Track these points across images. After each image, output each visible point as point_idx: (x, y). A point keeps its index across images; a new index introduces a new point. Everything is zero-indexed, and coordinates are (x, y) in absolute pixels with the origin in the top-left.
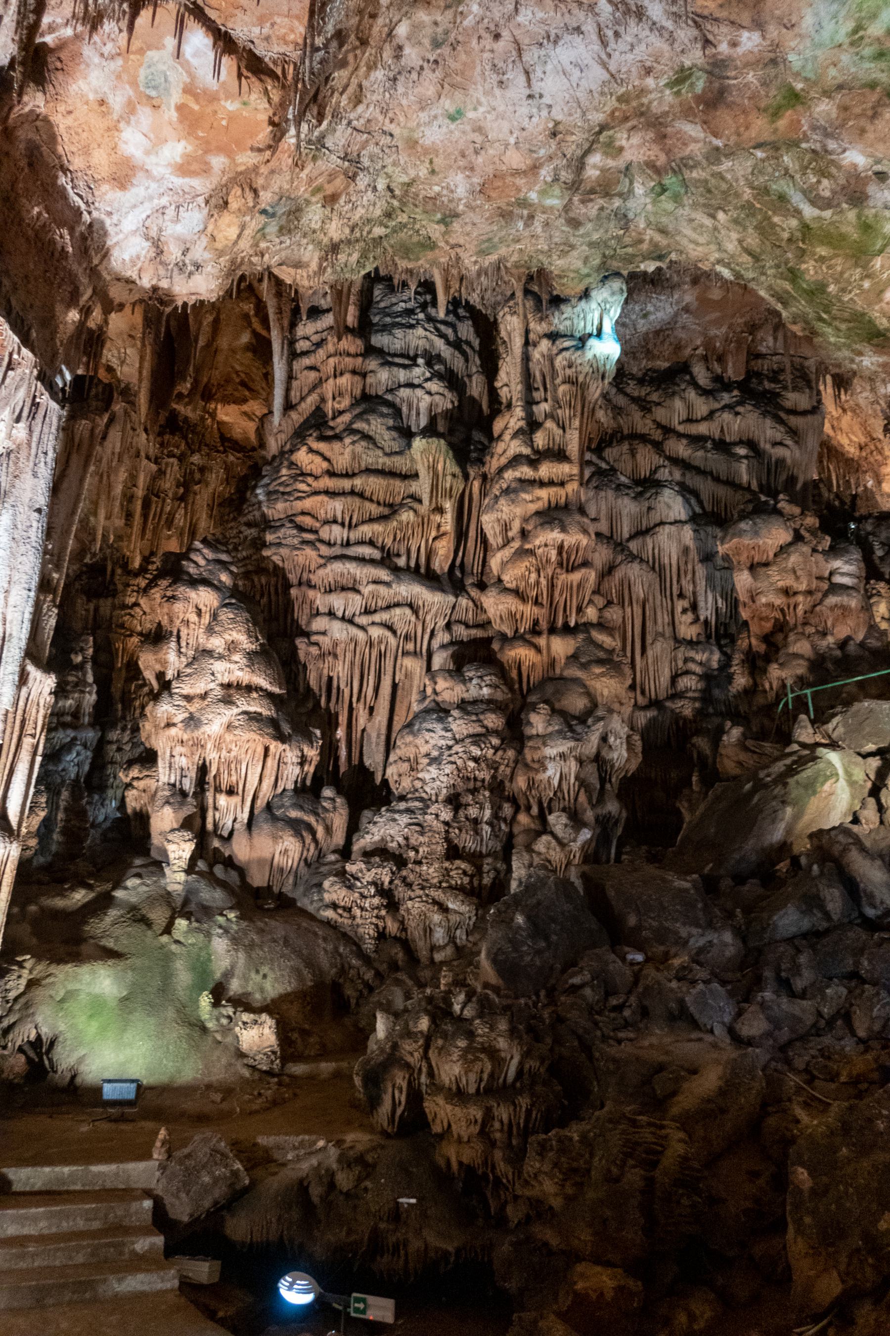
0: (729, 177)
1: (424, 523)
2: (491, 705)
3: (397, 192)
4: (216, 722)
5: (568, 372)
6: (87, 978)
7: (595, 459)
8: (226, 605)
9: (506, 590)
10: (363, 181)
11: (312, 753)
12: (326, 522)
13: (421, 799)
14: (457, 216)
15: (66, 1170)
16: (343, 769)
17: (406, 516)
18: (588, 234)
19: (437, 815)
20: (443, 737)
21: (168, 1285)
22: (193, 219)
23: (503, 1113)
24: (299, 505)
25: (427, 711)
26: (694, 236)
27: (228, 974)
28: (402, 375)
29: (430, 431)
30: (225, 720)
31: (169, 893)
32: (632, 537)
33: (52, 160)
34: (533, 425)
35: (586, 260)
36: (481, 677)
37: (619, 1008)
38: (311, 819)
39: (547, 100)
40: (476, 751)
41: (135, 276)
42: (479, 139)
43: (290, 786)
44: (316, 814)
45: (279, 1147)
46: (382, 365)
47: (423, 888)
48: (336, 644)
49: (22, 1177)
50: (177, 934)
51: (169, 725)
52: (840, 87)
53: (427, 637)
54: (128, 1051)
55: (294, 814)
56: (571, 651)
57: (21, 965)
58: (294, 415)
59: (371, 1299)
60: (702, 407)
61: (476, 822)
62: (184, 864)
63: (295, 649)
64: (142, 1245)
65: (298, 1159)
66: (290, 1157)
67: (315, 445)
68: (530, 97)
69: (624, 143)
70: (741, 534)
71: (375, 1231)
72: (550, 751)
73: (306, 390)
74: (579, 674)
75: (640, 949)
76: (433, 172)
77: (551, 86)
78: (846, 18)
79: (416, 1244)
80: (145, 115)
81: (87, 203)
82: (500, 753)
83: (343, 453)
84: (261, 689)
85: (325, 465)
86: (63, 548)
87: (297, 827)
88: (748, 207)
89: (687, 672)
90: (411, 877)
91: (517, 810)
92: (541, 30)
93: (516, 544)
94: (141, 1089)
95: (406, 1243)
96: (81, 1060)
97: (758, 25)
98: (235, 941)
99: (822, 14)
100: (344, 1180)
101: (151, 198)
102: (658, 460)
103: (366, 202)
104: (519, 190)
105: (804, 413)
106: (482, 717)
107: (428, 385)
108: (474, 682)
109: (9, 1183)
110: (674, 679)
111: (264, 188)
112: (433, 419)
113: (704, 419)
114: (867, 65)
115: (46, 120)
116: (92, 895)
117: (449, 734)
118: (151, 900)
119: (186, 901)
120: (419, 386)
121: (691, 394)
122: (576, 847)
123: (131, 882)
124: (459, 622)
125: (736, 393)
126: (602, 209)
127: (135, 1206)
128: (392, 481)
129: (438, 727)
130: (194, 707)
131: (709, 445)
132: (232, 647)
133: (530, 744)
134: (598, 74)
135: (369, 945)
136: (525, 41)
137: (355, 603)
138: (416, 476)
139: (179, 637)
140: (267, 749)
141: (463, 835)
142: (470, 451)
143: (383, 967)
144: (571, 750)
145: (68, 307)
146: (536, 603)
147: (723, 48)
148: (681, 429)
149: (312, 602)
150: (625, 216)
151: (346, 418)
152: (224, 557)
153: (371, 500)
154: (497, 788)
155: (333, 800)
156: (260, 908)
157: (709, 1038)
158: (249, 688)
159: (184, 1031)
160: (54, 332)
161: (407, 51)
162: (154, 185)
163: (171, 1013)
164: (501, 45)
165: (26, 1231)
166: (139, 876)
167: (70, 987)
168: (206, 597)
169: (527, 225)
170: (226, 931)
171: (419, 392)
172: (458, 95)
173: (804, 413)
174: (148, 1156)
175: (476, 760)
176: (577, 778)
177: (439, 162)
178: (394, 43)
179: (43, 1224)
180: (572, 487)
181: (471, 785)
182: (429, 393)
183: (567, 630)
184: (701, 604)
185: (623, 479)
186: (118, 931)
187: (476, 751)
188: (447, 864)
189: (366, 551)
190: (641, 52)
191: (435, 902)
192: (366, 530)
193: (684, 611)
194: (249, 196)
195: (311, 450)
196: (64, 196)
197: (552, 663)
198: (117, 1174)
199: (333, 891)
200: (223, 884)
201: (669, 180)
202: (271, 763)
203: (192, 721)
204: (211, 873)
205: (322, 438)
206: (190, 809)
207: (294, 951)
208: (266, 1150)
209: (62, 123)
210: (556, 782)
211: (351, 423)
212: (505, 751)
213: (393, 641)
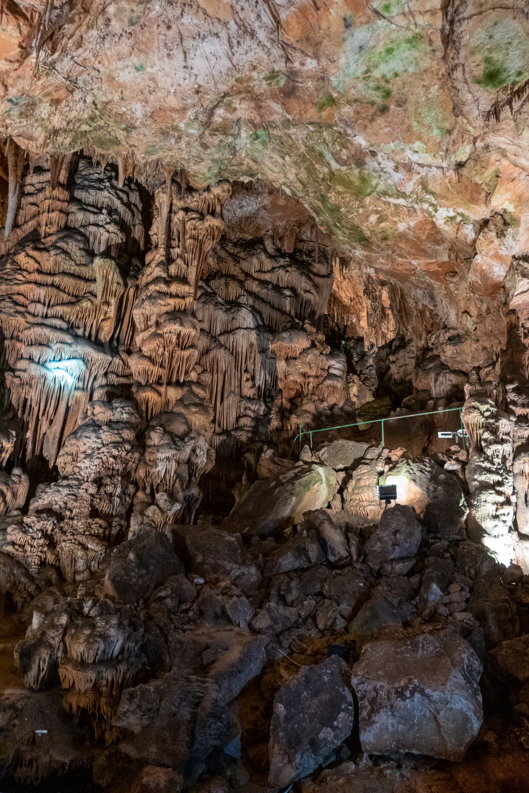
0: (294, 137)
2: (128, 425)
3: (99, 106)
5: (194, 232)
7: (204, 285)
10: (77, 95)
12: (33, 301)
13: (77, 480)
16: (28, 457)
17: (86, 304)
18: (211, 154)
19: (86, 490)
24: (16, 288)
25: (87, 425)
26: (272, 167)
28: (92, 218)
29: (106, 254)
32: (219, 335)
34: (169, 260)
35: (209, 169)
39: (195, 71)
40: (115, 452)
42: (152, 85)
44: (7, 485)
46: (80, 210)
47: (73, 535)
48: (32, 378)
52: (356, 101)
53: (91, 380)
56: (179, 397)
58: (19, 231)
60: (268, 264)
67: (31, 252)
68: (185, 67)
69: (237, 106)
70: (283, 339)
73: (28, 217)
74: (183, 411)
75: (202, 576)
76: (122, 99)
77: (198, 64)
82: (130, 454)
83: (49, 260)
85: (36, 266)
88: (302, 156)
89: (245, 416)
90: (66, 528)
91: (137, 489)
92: (195, 30)
97: (316, 56)
102: (240, 291)
103: (78, 109)
104: (174, 120)
105: (323, 276)
106: (121, 432)
108: (119, 410)
110: (238, 419)
113: (269, 271)
114: (371, 92)
117: (99, 441)
120: (102, 226)
121: (263, 256)
122: (171, 513)
124: (113, 372)
125: (287, 259)
128: (79, 282)
129: (93, 435)
131: (270, 287)
133: (149, 450)
135: (34, 569)
136: (185, 34)
138: (95, 280)
146: (161, 366)
147: (297, 65)
148: (255, 275)
150: (234, 148)
151: (53, 238)
153: (64, 292)
155: (19, 476)
157: (237, 629)
161: (113, 22)
169: (176, 142)
171: (101, 230)
172: (142, 56)
173: (323, 276)
175: (115, 457)
177: (127, 93)
178: (106, 16)
180: (189, 300)
181: (110, 473)
182: (108, 232)
183: (178, 384)
184: (257, 377)
187: (115, 452)
188: (90, 520)
190: (251, 56)
191: (80, 544)
192: (59, 310)
193: (247, 380)
195: (28, 255)
197: (167, 403)
201: (260, 132)
205: (36, 249)
210: (162, 474)
211: (56, 242)
212: (133, 453)
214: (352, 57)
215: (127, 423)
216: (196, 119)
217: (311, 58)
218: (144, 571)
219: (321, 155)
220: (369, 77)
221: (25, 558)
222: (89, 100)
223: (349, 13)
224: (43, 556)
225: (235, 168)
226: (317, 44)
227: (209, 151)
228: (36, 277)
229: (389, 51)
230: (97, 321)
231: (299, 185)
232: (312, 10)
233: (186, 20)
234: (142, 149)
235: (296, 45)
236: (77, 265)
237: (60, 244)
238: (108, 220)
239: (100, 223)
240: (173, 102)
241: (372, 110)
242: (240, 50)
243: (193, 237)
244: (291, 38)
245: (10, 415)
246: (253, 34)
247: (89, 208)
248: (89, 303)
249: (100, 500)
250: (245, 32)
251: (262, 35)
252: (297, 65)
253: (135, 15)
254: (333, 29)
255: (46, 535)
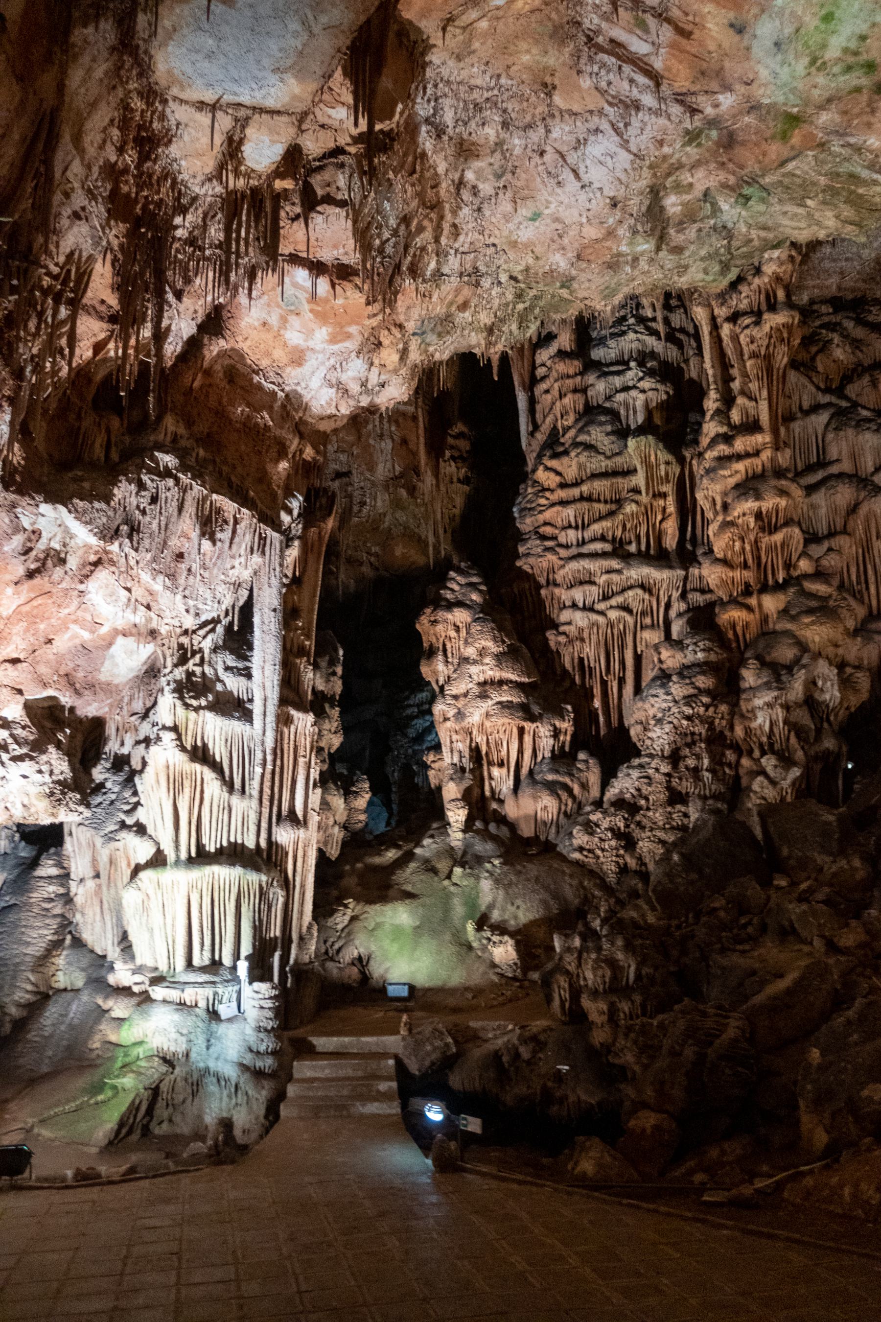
0: (798, 172)
1: (648, 511)
2: (703, 667)
3: (520, 277)
4: (475, 716)
5: (753, 347)
6: (390, 913)
7: (834, 400)
8: (475, 621)
9: (717, 560)
10: (486, 283)
11: (566, 725)
12: (564, 528)
14: (573, 279)
15: (346, 1039)
16: (602, 733)
18: (694, 253)
19: (657, 770)
20: (665, 701)
21: (394, 1111)
22: (356, 368)
23: (625, 1006)
24: (541, 518)
26: (794, 224)
27: (491, 907)
28: (617, 381)
29: (641, 431)
30: (483, 711)
31: (452, 848)
33: (246, 370)
34: (728, 400)
35: (706, 271)
36: (695, 644)
37: (745, 926)
38: (567, 780)
39: (596, 185)
40: (688, 711)
41: (334, 411)
42: (559, 227)
43: (548, 754)
44: (571, 775)
45: (483, 1029)
46: (599, 377)
47: (652, 830)
48: (581, 630)
49: (322, 1043)
50: (455, 879)
51: (446, 719)
52: (829, 100)
53: (662, 610)
54: (417, 964)
55: (550, 777)
56: (782, 606)
57: (346, 906)
59: (470, 1118)
61: (696, 771)
62: (461, 826)
63: (547, 640)
64: (383, 1086)
65: (496, 1037)
66: (490, 1035)
68: (583, 187)
69: (690, 180)
71: (544, 1086)
72: (758, 702)
74: (789, 626)
76: (537, 258)
77: (595, 175)
78: (796, 57)
79: (572, 1098)
80: (294, 320)
81: (279, 385)
82: (711, 709)
83: (570, 467)
84: (511, 682)
85: (558, 479)
86: (310, 623)
87: (552, 788)
88: (828, 189)
90: (645, 821)
91: (740, 756)
92: (572, 139)
93: (720, 518)
94: (412, 988)
95: (566, 1097)
96: (387, 970)
97: (727, 88)
98: (497, 881)
99: (772, 65)
100: (525, 1052)
101: (323, 363)
103: (497, 295)
104: (610, 249)
107: (641, 385)
109: (314, 1046)
111: (407, 320)
112: (649, 412)
114: (842, 79)
115: (233, 349)
116: (400, 853)
118: (439, 855)
119: (465, 853)
120: (634, 387)
122: (786, 784)
123: (426, 842)
124: (695, 590)
126: (700, 230)
127: (383, 1063)
128: (614, 480)
129: (661, 692)
130: (461, 703)
132: (482, 652)
134: (624, 158)
135: (612, 878)
136: (564, 149)
137: (593, 592)
138: (635, 470)
139: (445, 651)
140: (521, 731)
141: (684, 783)
142: (687, 434)
143: (623, 896)
144: (776, 698)
145: (277, 461)
146: (745, 566)
147: (709, 111)
149: (559, 599)
150: (724, 227)
151: (572, 433)
152: (475, 579)
153: (599, 501)
154: (717, 741)
155: (586, 761)
156: (525, 854)
157: (806, 949)
158: (501, 682)
159: (454, 949)
160: (269, 484)
161: (481, 186)
162: (320, 356)
163: (447, 937)
164: (547, 157)
165: (318, 1075)
166: (432, 836)
167: (378, 920)
168: (461, 616)
169: (633, 267)
170: (491, 874)
171: (634, 393)
172: (529, 203)
174: (397, 1033)
175: (689, 718)
176: (785, 723)
177: (539, 250)
179: (327, 1071)
180: (766, 455)
181: (689, 739)
182: (643, 391)
183: (779, 588)
185: (865, 413)
186: (415, 878)
188: (669, 809)
189: (598, 546)
190: (648, 133)
192: (597, 528)
194: (396, 331)
195: (547, 468)
196: (259, 387)
197: (765, 619)
198: (377, 1044)
199: (580, 838)
200: (494, 838)
201: (747, 191)
202: (528, 739)
203: (460, 715)
204: (486, 829)
205: (556, 456)
206: (467, 783)
207: (544, 887)
208: (475, 1030)
209: (244, 346)
210: (767, 728)
212: (716, 707)
213: (630, 620)
214: (774, 62)
215: (706, 663)
216: (635, 232)
217: (722, 93)
218: (694, 876)
219: (852, 176)
220: (824, 63)
221: (600, 865)
222: (504, 278)
223: (731, 15)
224: (621, 861)
225: (745, 249)
226: (719, 73)
227: (687, 253)
228: (562, 494)
229: (828, 18)
230: (654, 525)
231: (849, 228)
232: (683, 42)
233: (556, 134)
234: (596, 296)
235: (693, 89)
236: (608, 458)
237: (582, 438)
238: (641, 374)
239: (631, 384)
240: (592, 232)
241: (864, 98)
242: (632, 131)
243: (754, 355)
244: (683, 84)
245: (567, 684)
246: (637, 106)
247: (612, 369)
248: (634, 506)
249: (680, 779)
250: (627, 106)
251: (648, 100)
252: (709, 111)
253: (496, 167)
254: (726, 44)
255: (617, 834)
